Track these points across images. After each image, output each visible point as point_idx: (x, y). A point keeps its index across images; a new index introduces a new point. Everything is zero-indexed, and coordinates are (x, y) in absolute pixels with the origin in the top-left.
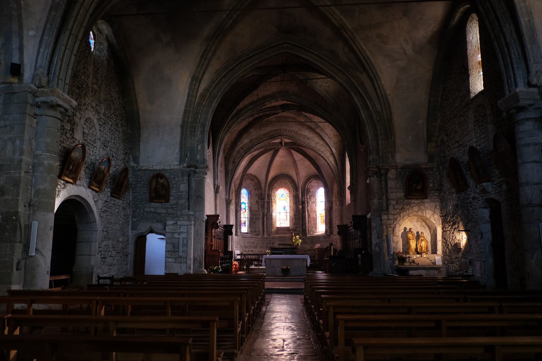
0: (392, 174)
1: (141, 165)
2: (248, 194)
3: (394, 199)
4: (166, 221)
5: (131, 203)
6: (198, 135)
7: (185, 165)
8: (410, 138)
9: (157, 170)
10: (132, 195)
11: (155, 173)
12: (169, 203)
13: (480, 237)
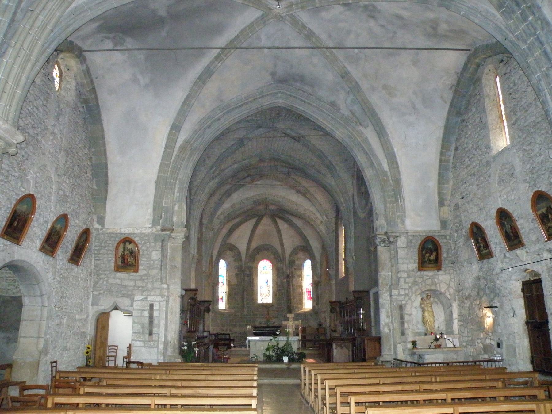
0: (401, 242)
1: (106, 226)
3: (404, 271)
4: (135, 295)
5: (92, 273)
6: (176, 193)
7: (159, 228)
8: (421, 201)
9: (125, 234)
10: (94, 263)
11: (123, 237)
12: (138, 274)
13: (512, 315)
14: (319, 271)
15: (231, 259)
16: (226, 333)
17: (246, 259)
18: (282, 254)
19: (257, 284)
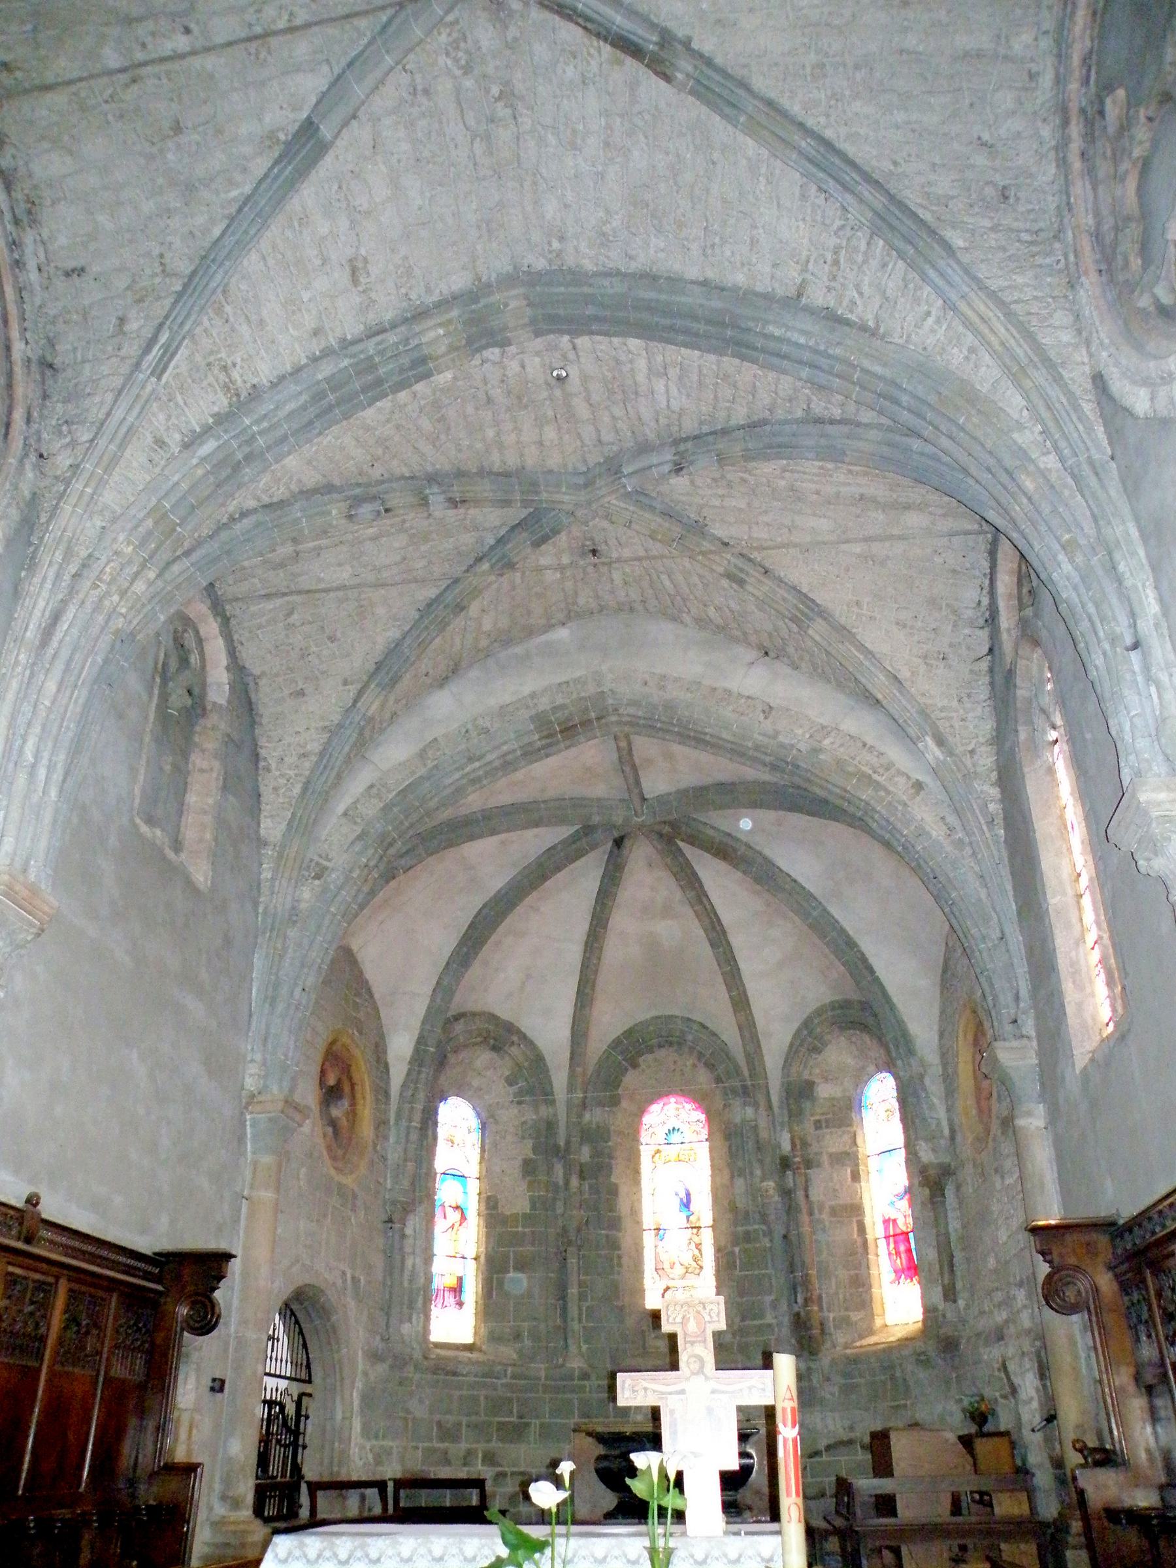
2: (483, 1127)
14: (942, 1114)
15: (501, 1092)
16: (462, 1474)
17: (571, 1088)
18: (748, 1056)
19: (635, 1213)
